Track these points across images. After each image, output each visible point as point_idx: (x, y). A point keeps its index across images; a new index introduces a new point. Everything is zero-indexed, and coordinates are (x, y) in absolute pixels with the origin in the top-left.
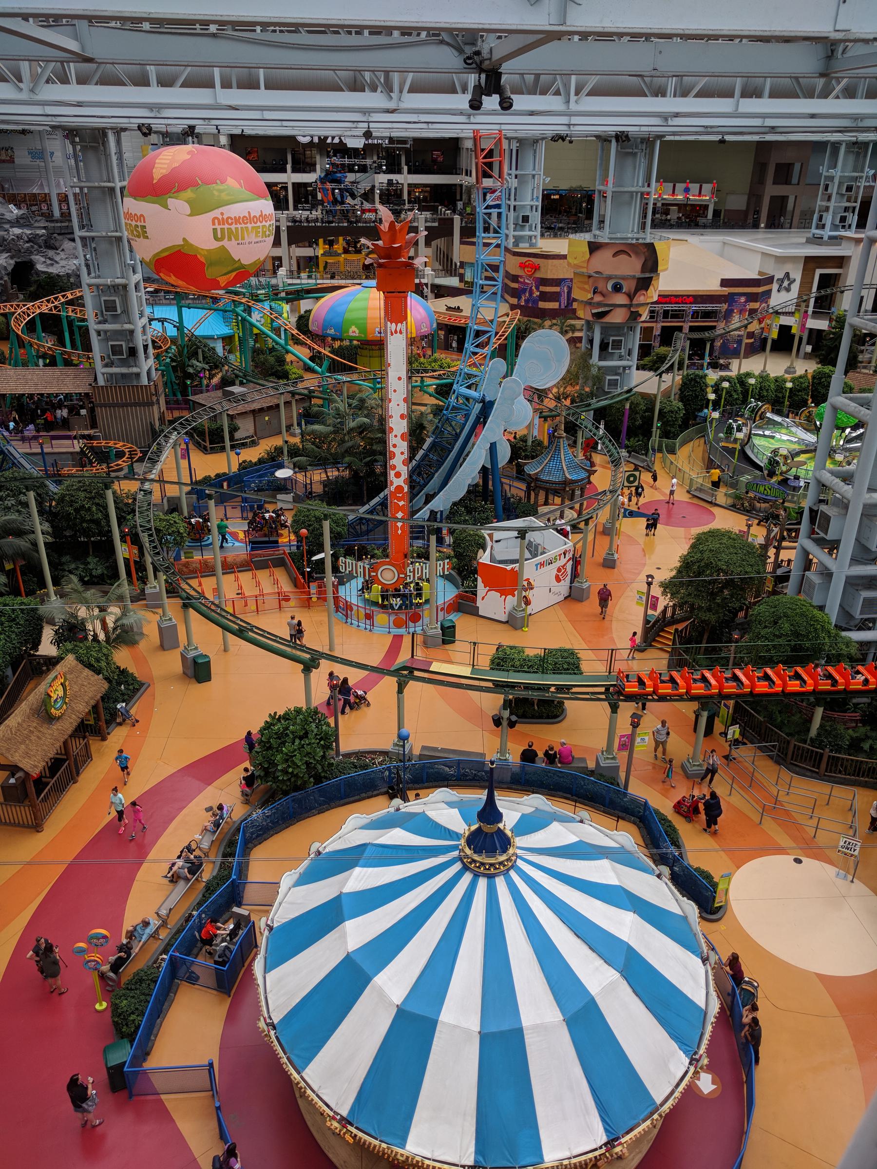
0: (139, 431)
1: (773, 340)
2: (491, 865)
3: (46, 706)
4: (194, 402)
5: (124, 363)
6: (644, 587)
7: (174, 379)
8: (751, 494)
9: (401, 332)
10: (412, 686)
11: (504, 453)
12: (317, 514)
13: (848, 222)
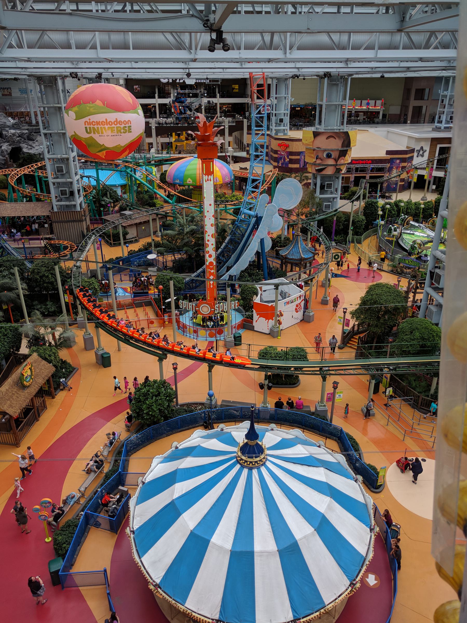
1: (415, 183)
4: (105, 220)
5: (67, 199)
7: (94, 208)
8: (401, 265)
11: (268, 245)
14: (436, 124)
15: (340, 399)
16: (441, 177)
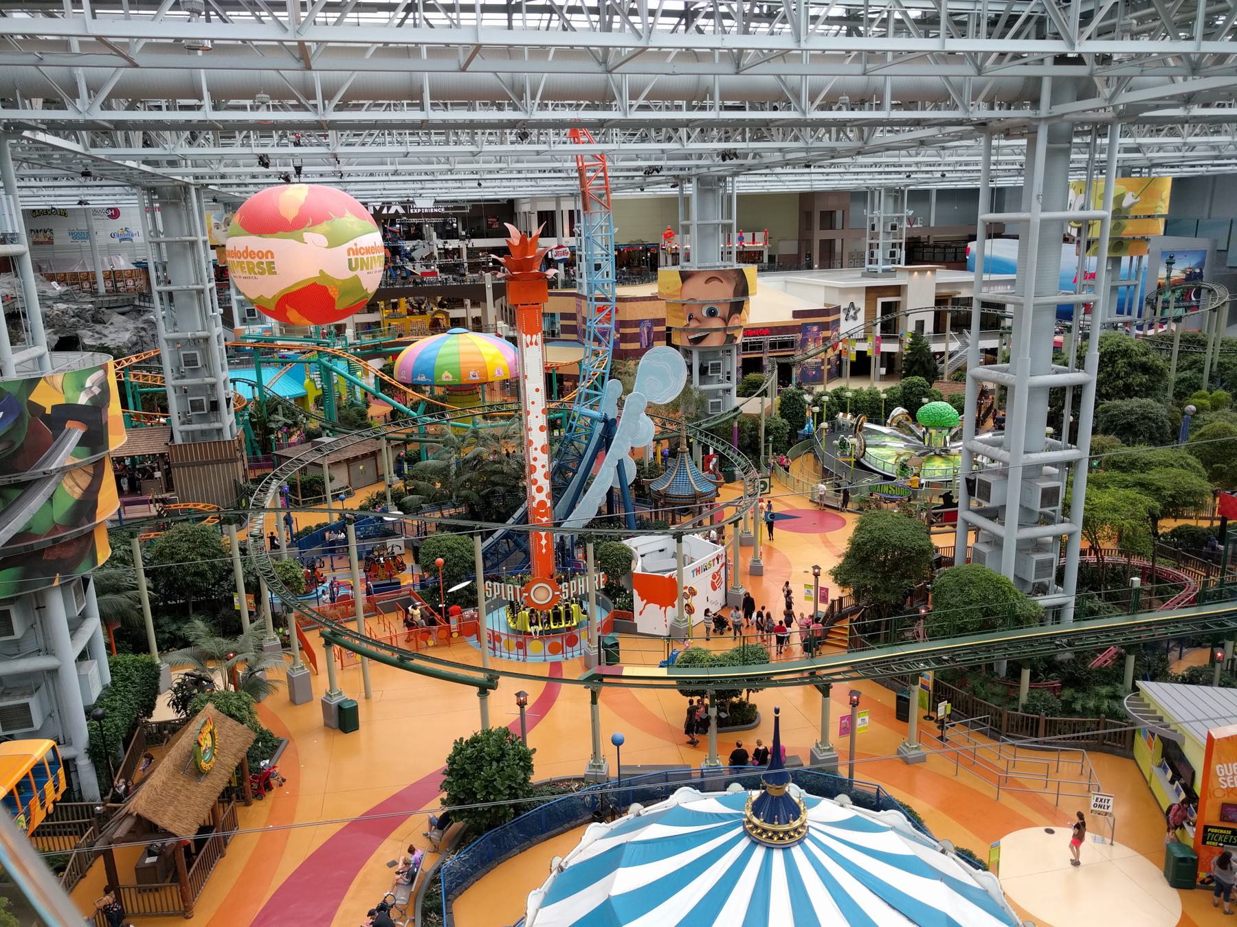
0: (221, 489)
1: (852, 363)
2: (786, 832)
3: (195, 757)
5: (203, 418)
6: (811, 580)
7: (253, 437)
9: (536, 344)
10: (605, 692)
11: (631, 473)
12: (449, 543)
14: (867, 266)
15: (866, 728)
16: (894, 353)
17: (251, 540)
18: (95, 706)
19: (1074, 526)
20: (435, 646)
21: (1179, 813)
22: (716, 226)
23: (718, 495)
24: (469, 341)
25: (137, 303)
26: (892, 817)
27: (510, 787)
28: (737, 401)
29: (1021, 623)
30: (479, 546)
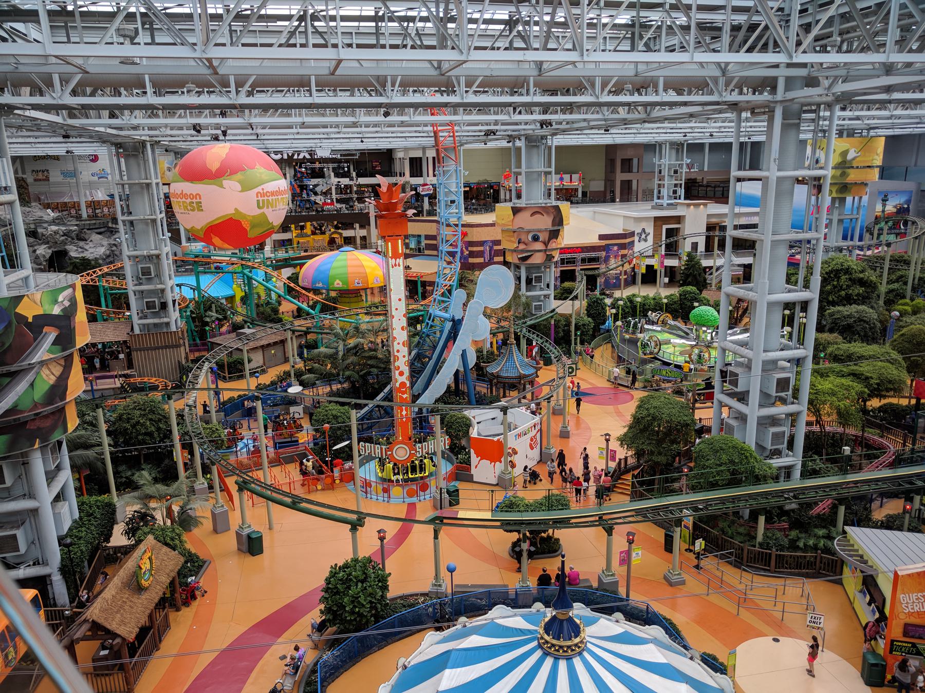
1: (642, 274)
2: (569, 647)
4: (212, 343)
5: (156, 315)
8: (656, 378)
11: (472, 360)
12: (334, 412)
13: (678, 193)
14: (656, 200)
16: (675, 267)
17: (187, 409)
18: (66, 536)
19: (802, 407)
20: (323, 490)
21: (874, 629)
22: (539, 173)
23: (537, 376)
24: (354, 257)
25: (110, 225)
26: (656, 631)
27: (371, 602)
28: (554, 304)
29: (760, 480)
30: (354, 415)
